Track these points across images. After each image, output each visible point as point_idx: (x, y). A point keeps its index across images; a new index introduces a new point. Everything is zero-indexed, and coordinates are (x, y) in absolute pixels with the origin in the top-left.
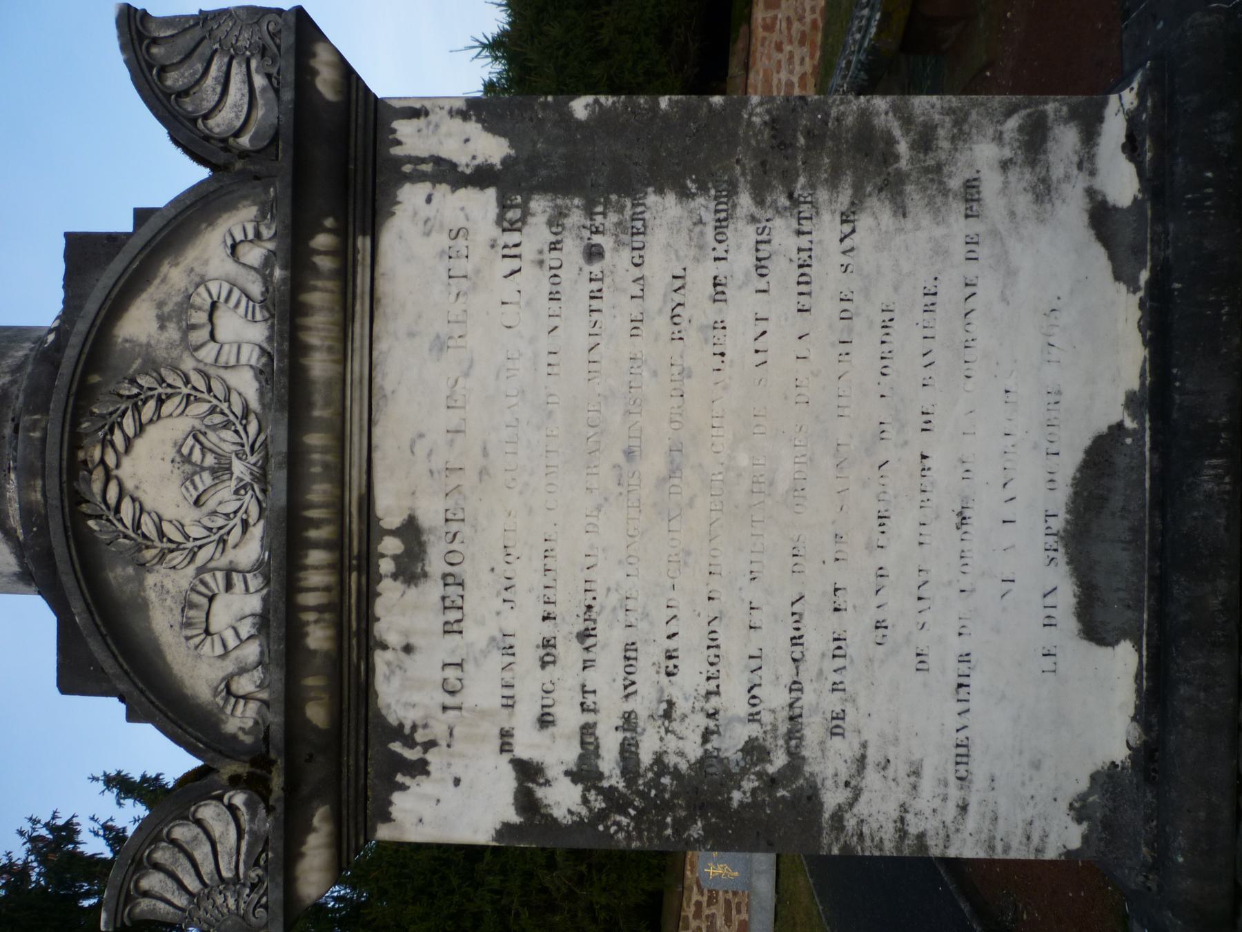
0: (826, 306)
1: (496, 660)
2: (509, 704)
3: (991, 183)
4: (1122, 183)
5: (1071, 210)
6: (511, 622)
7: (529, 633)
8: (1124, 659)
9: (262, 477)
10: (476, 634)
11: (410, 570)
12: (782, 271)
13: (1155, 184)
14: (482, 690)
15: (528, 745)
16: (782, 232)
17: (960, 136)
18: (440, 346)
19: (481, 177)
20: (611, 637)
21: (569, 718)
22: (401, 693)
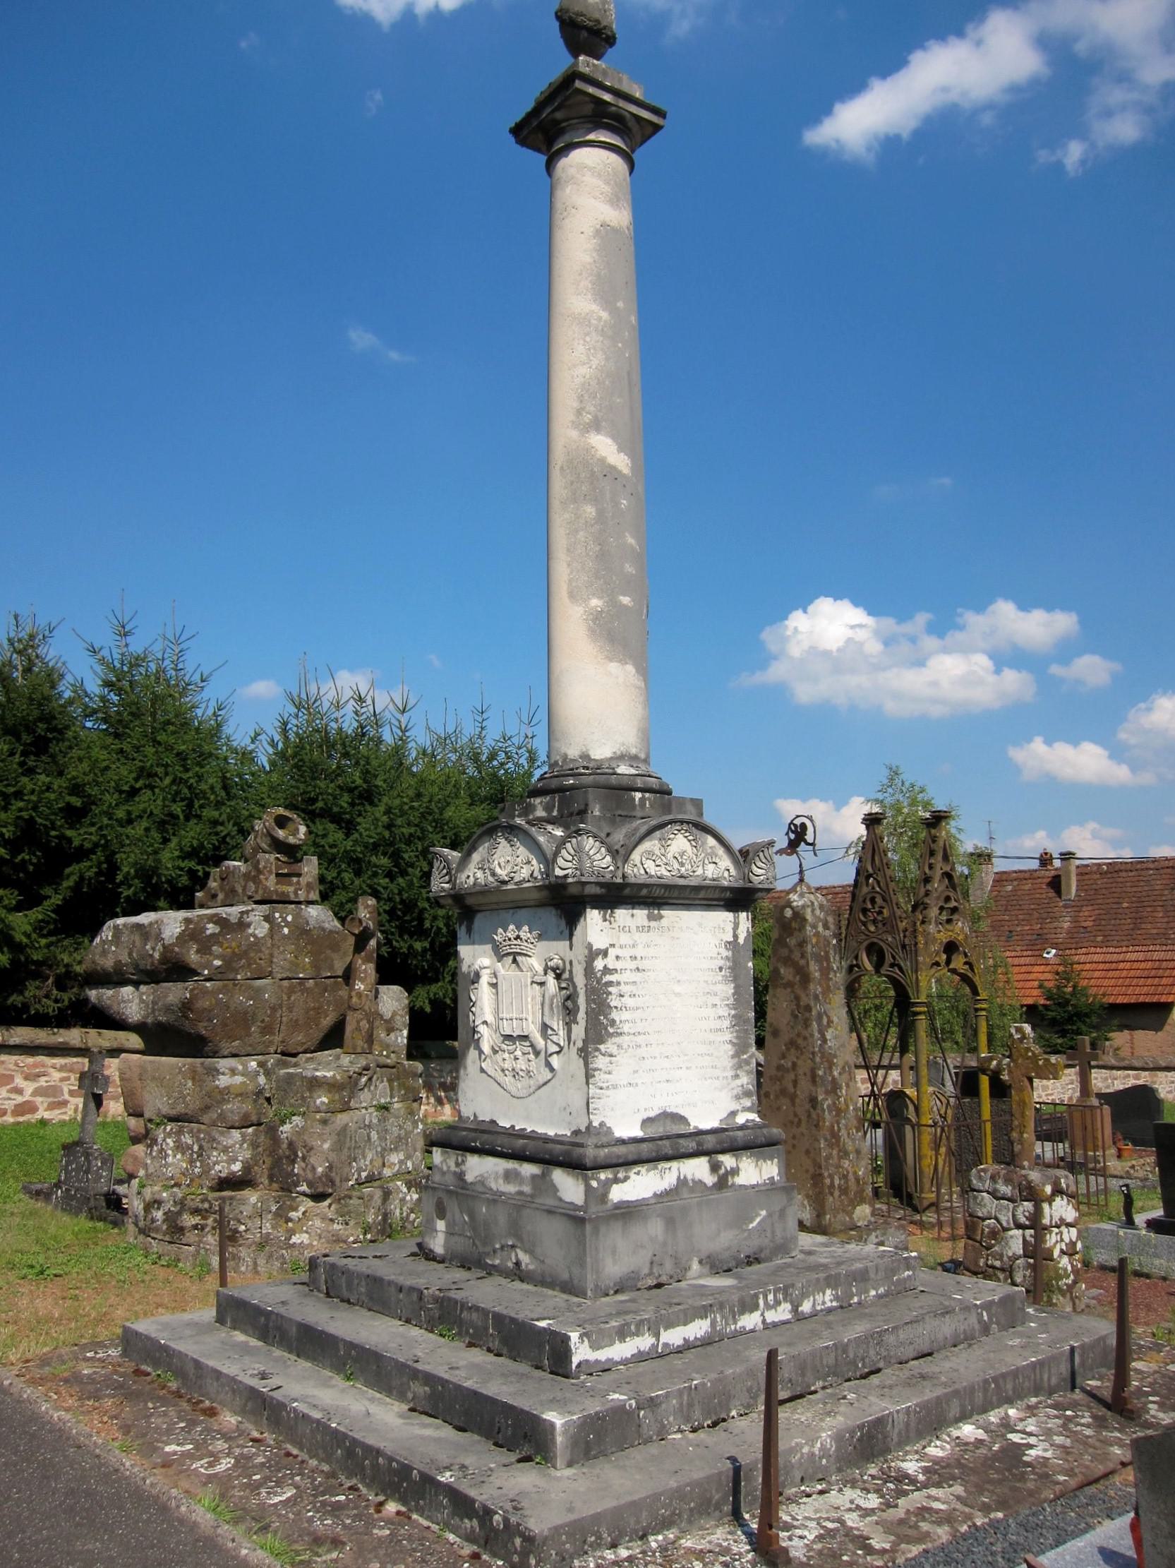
0: (712, 1037)
1: (631, 943)
2: (621, 947)
3: (739, 1082)
4: (741, 1119)
5: (734, 1106)
6: (640, 946)
7: (639, 952)
8: (638, 1133)
9: (681, 877)
10: (637, 936)
11: (650, 918)
12: (718, 1024)
13: (742, 1128)
14: (624, 939)
15: (612, 952)
16: (727, 1023)
17: (748, 1073)
18: (700, 925)
19: (736, 936)
20: (636, 977)
21: (618, 965)
22: (622, 914)
